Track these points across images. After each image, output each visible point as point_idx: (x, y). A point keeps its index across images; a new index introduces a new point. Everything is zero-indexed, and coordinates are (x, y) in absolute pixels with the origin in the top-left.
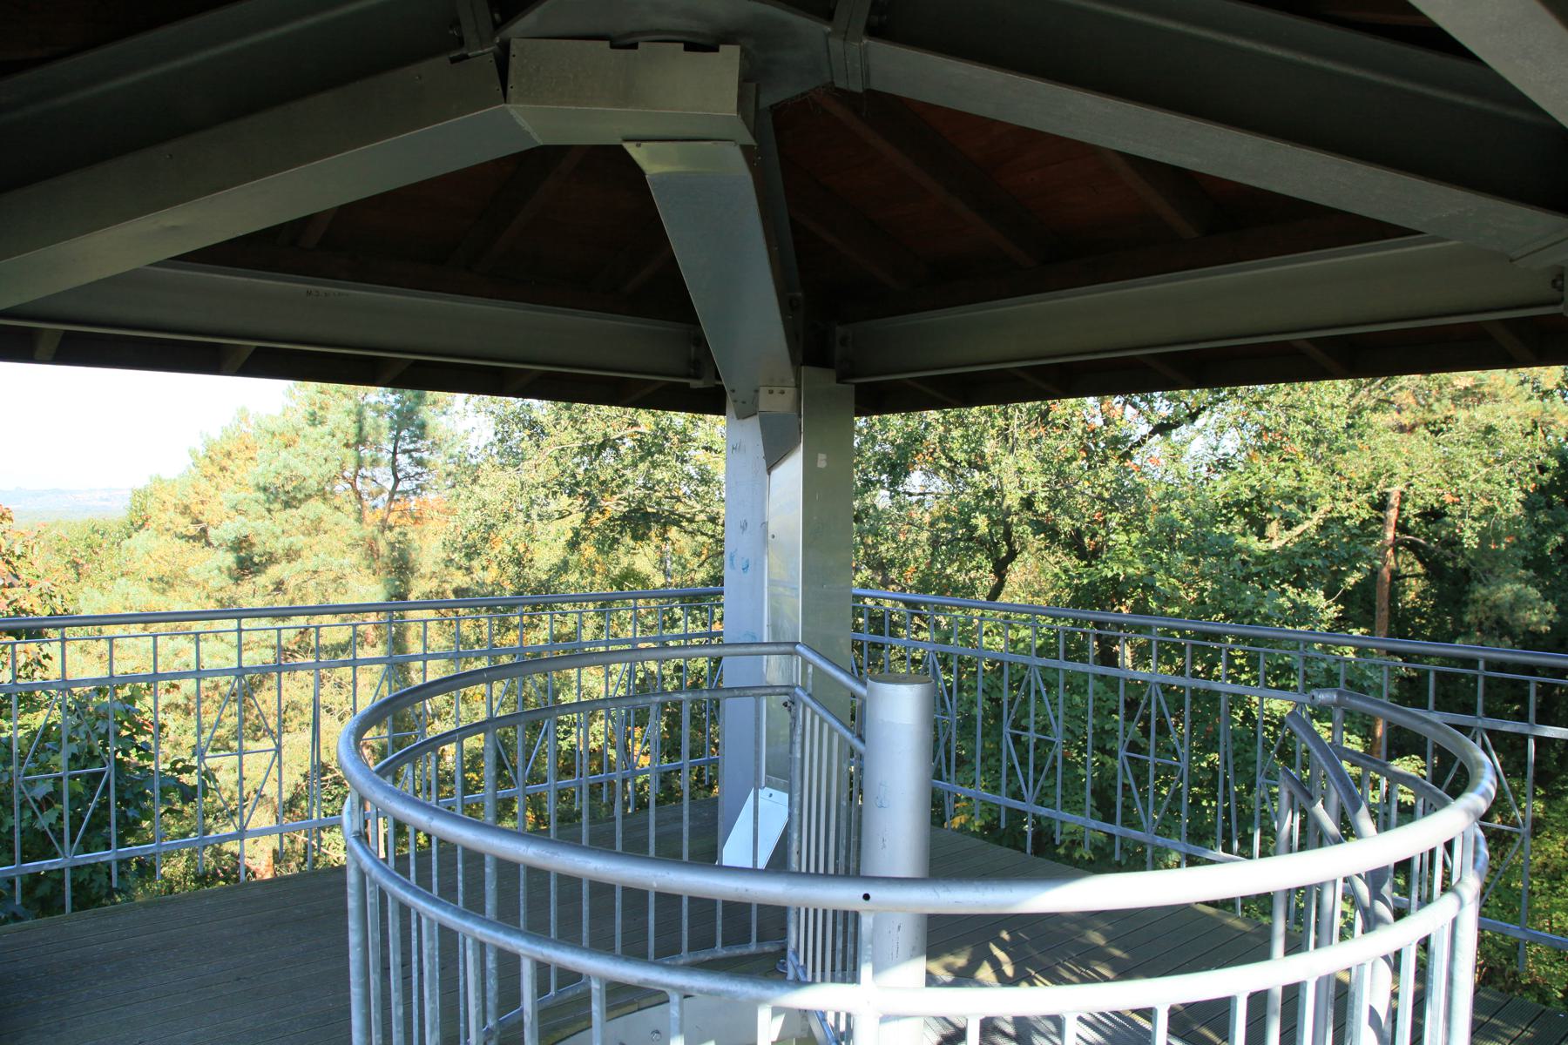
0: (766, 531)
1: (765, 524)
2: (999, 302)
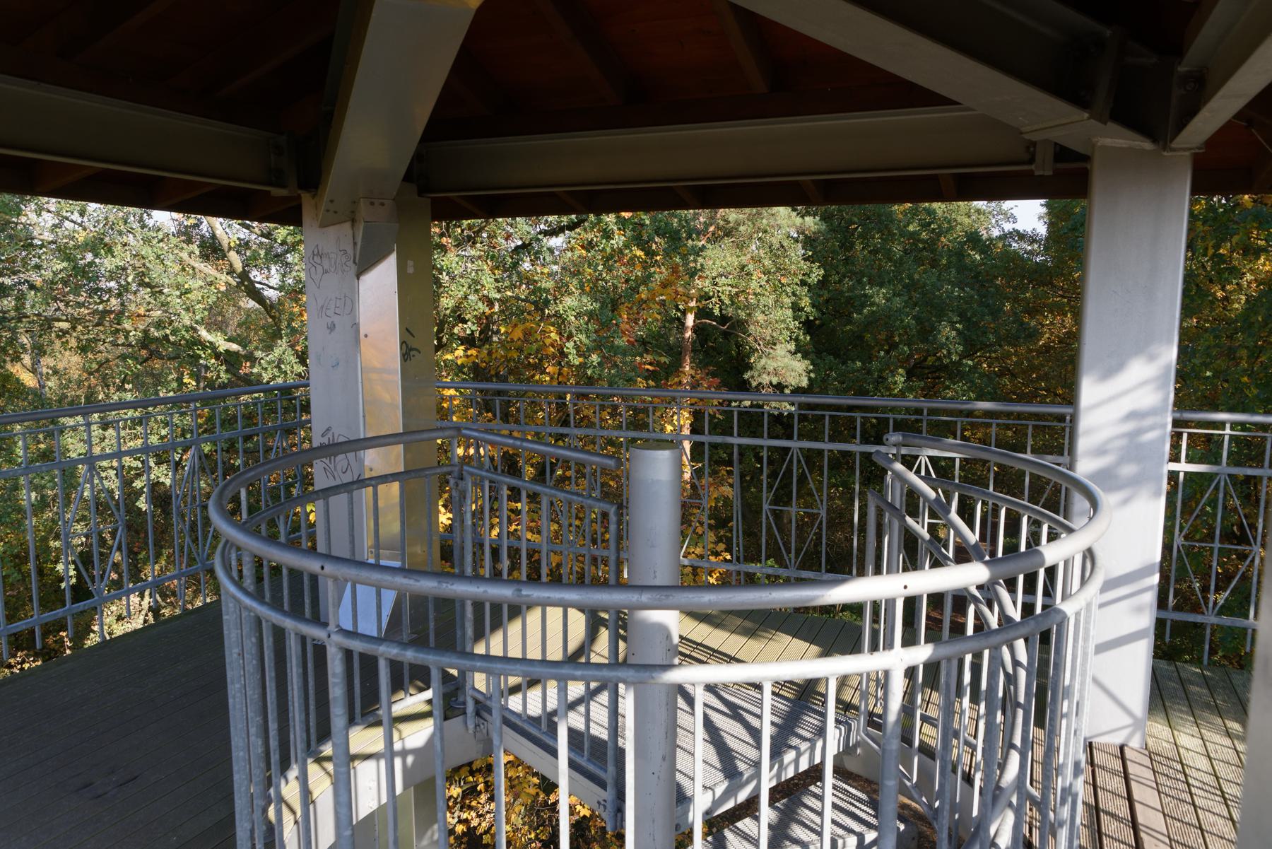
0: (358, 331)
1: (356, 326)
2: (623, 130)
